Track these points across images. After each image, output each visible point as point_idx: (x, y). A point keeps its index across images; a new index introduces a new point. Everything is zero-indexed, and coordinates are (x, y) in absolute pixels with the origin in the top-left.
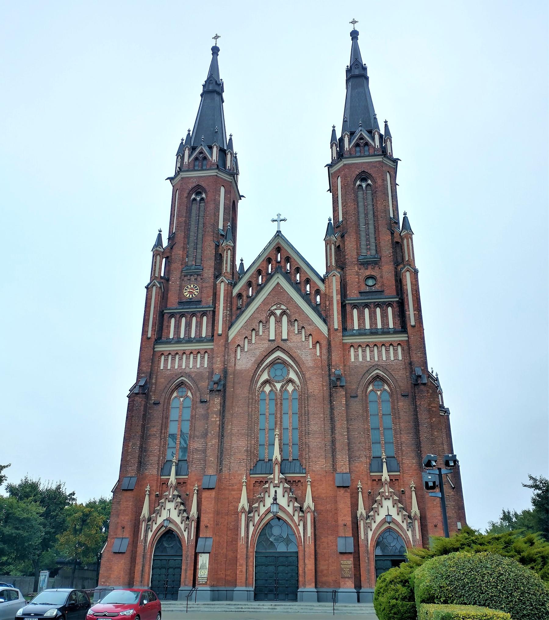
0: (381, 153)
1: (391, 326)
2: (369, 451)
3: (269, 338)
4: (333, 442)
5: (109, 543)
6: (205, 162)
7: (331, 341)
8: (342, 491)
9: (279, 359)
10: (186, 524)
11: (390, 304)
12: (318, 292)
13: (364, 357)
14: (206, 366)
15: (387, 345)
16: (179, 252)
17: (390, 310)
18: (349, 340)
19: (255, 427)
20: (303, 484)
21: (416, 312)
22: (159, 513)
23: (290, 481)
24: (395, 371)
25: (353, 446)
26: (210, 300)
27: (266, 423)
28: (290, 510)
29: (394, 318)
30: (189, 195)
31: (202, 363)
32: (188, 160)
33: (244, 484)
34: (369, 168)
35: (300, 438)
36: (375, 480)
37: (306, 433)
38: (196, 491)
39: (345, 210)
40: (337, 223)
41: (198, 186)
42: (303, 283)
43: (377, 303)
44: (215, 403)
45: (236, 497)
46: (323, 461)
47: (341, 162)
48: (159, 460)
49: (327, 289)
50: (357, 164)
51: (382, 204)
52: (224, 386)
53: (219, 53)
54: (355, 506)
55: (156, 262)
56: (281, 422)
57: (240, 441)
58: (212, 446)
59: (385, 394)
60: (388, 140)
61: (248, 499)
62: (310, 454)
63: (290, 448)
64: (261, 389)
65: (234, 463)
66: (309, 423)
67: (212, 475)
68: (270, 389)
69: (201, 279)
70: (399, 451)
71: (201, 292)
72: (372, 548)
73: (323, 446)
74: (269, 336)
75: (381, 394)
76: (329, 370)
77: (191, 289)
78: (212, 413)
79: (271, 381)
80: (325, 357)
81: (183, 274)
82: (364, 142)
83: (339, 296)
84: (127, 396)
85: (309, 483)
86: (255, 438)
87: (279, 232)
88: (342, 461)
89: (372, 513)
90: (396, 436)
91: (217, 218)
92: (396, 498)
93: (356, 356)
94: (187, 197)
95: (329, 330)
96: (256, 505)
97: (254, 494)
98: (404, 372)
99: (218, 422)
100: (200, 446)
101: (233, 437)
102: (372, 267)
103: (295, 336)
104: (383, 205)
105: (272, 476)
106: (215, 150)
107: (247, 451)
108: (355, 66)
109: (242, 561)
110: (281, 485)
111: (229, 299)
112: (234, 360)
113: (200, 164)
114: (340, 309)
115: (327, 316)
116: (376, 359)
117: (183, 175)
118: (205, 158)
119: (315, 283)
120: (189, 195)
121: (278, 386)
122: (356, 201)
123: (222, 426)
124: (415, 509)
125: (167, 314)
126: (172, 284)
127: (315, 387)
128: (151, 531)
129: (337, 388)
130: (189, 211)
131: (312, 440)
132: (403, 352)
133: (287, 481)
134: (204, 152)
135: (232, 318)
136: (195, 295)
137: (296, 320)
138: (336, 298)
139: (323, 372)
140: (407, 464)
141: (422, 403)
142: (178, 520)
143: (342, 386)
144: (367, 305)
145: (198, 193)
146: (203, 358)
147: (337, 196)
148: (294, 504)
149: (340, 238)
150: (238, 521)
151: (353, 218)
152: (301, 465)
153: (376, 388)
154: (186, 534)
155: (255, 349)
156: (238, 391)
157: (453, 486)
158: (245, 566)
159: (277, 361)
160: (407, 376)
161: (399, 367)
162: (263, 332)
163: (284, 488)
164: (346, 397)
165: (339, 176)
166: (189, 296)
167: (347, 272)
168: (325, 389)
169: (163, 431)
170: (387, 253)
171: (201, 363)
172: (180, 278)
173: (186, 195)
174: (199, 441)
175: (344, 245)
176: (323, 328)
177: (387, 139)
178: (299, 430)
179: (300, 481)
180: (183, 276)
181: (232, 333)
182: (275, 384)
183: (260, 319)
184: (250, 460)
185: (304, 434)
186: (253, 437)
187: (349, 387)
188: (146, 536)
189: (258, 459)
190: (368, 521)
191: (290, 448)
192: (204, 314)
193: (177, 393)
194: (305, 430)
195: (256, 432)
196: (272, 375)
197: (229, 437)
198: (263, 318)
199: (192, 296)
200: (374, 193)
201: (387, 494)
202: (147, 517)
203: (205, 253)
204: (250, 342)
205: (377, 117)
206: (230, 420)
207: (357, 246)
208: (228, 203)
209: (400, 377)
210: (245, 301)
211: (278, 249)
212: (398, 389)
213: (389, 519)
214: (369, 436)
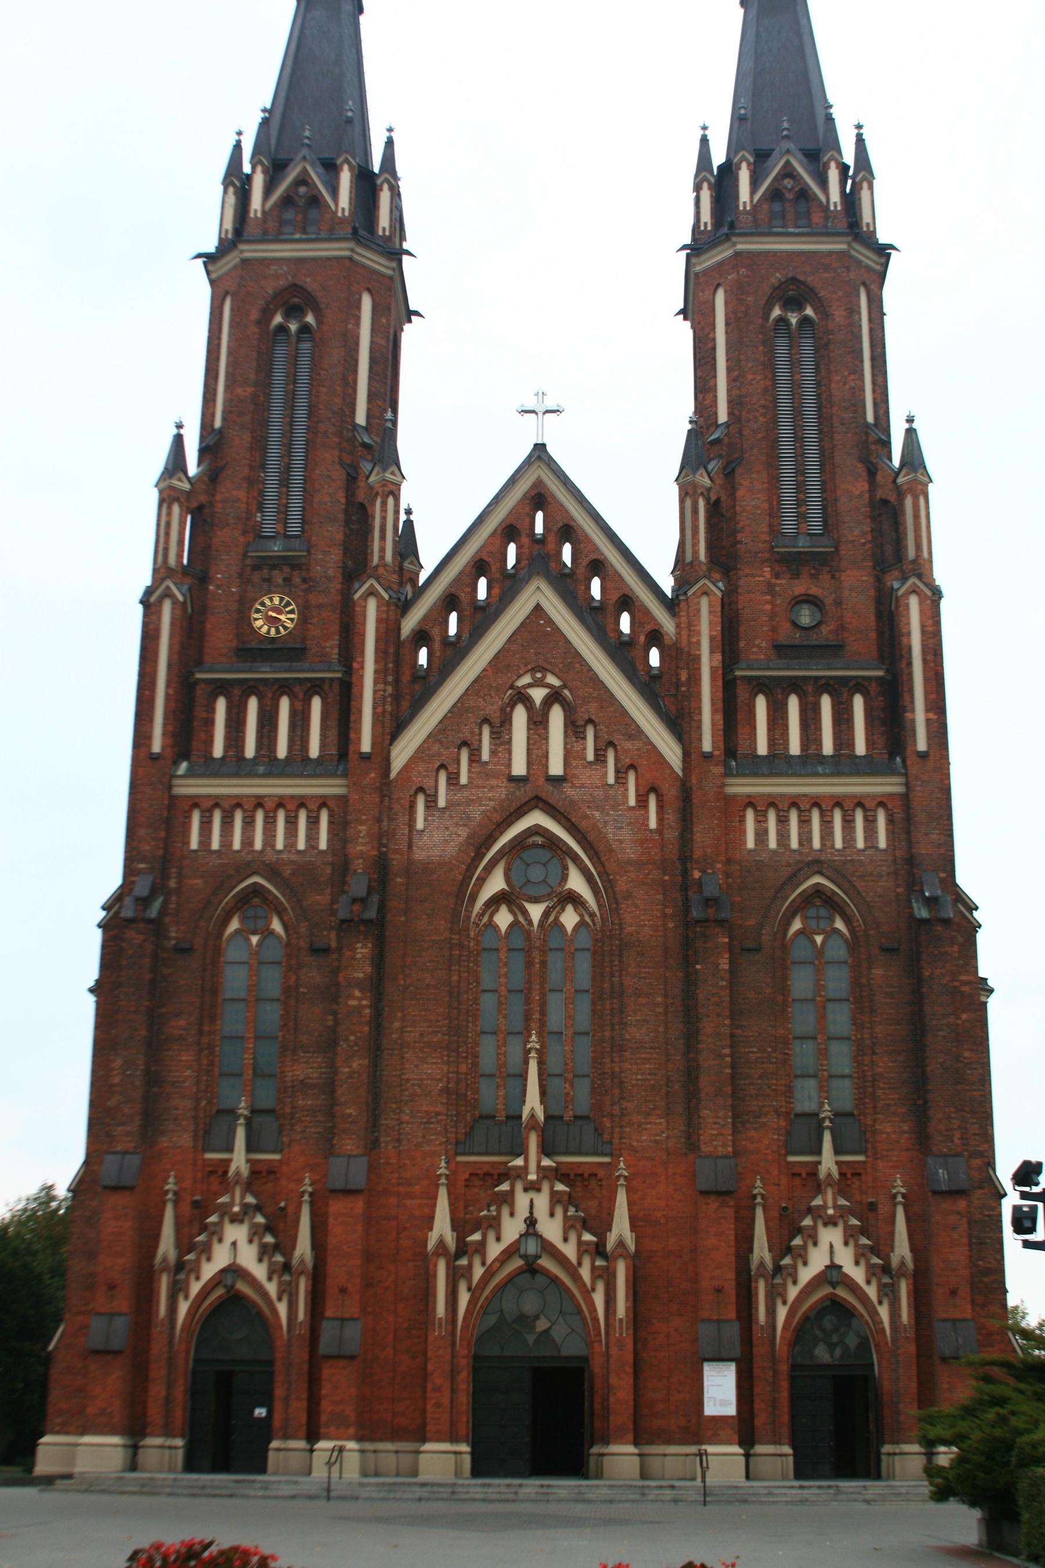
1: (860, 748)
2: (786, 1097)
3: (510, 772)
4: (691, 1073)
6: (313, 213)
7: (691, 788)
8: (713, 1204)
9: (537, 833)
10: (280, 1284)
11: (859, 686)
12: (655, 637)
14: (323, 845)
15: (848, 805)
16: (235, 493)
17: (316, 703)
18: (741, 787)
19: (467, 1027)
20: (603, 1183)
21: (931, 716)
22: (206, 1251)
23: (568, 1175)
24: (866, 878)
25: (745, 1084)
26: (332, 647)
27: (500, 1016)
30: (267, 314)
32: (263, 205)
33: (443, 1180)
35: (594, 1060)
36: (800, 1175)
38: (306, 1197)
41: (295, 288)
42: (551, 538)
43: (823, 681)
44: (359, 956)
46: (661, 1123)
47: (726, 245)
48: (196, 1108)
49: (684, 632)
50: (774, 254)
51: (845, 384)
52: (382, 908)
54: (745, 1242)
55: (168, 524)
56: (543, 1013)
57: (427, 1063)
58: (351, 1077)
59: (836, 943)
60: (865, 185)
61: (453, 1220)
62: (625, 1104)
63: (567, 1085)
64: (485, 919)
65: (412, 1123)
66: (625, 1020)
67: (354, 1156)
69: (304, 580)
70: (867, 1100)
71: (304, 620)
72: (785, 1348)
73: (662, 1082)
74: (509, 765)
76: (685, 873)
77: (275, 609)
79: (514, 898)
80: (672, 835)
81: (248, 562)
82: (797, 189)
83: (718, 657)
85: (622, 1181)
86: (470, 1057)
87: (540, 449)
88: (715, 1126)
89: (787, 1261)
90: (860, 1058)
91: (350, 391)
92: (854, 1222)
93: (761, 835)
94: (258, 322)
95: (686, 755)
96: (476, 1237)
97: (466, 1207)
100: (312, 1073)
101: (407, 1053)
102: (813, 571)
103: (587, 767)
104: (847, 387)
105: (519, 1162)
106: (345, 178)
107: (446, 1091)
109: (438, 1379)
110: (546, 1187)
111: (391, 650)
112: (406, 832)
113: (300, 217)
116: (816, 844)
117: (250, 251)
118: (315, 200)
119: (647, 612)
120: (267, 314)
121: (535, 912)
122: (769, 366)
123: (377, 1022)
124: (902, 1249)
125: (203, 685)
127: (643, 920)
129: (707, 924)
130: (266, 366)
131: (629, 1067)
132: (890, 827)
133: (559, 1174)
134: (310, 181)
135: (398, 704)
136: (285, 628)
137: (590, 721)
139: (667, 878)
140: (888, 1133)
141: (938, 972)
143: (720, 922)
144: (795, 686)
147: (710, 345)
148: (579, 1237)
149: (721, 476)
150: (429, 1279)
151: (762, 419)
152: (598, 1132)
154: (282, 1308)
155: (469, 802)
158: (447, 1393)
159: (531, 840)
160: (898, 895)
162: (493, 753)
163: (553, 1194)
164: (731, 952)
165: (719, 285)
166: (268, 632)
167: (741, 583)
168: (671, 925)
169: (206, 1028)
170: (856, 532)
172: (241, 575)
173: (255, 314)
174: (311, 1060)
175: (734, 499)
176: (671, 751)
177: (861, 182)
178: (593, 1036)
179: (596, 1175)
181: (402, 753)
184: (456, 1115)
185: (608, 1050)
186: (464, 1055)
187: (739, 922)
188: (173, 1309)
189: (477, 1113)
190: (778, 1280)
191: (567, 1085)
192: (315, 687)
193: (241, 922)
195: (470, 1040)
196: (518, 880)
197: (395, 1052)
198: (492, 710)
199: (278, 631)
200: (821, 349)
201: (830, 1212)
203: (316, 500)
204: (453, 779)
205: (835, 112)
206: (399, 1004)
207: (771, 504)
208: (383, 342)
209: (880, 896)
210: (438, 654)
211: (538, 499)
212: (872, 932)
214: (786, 1057)
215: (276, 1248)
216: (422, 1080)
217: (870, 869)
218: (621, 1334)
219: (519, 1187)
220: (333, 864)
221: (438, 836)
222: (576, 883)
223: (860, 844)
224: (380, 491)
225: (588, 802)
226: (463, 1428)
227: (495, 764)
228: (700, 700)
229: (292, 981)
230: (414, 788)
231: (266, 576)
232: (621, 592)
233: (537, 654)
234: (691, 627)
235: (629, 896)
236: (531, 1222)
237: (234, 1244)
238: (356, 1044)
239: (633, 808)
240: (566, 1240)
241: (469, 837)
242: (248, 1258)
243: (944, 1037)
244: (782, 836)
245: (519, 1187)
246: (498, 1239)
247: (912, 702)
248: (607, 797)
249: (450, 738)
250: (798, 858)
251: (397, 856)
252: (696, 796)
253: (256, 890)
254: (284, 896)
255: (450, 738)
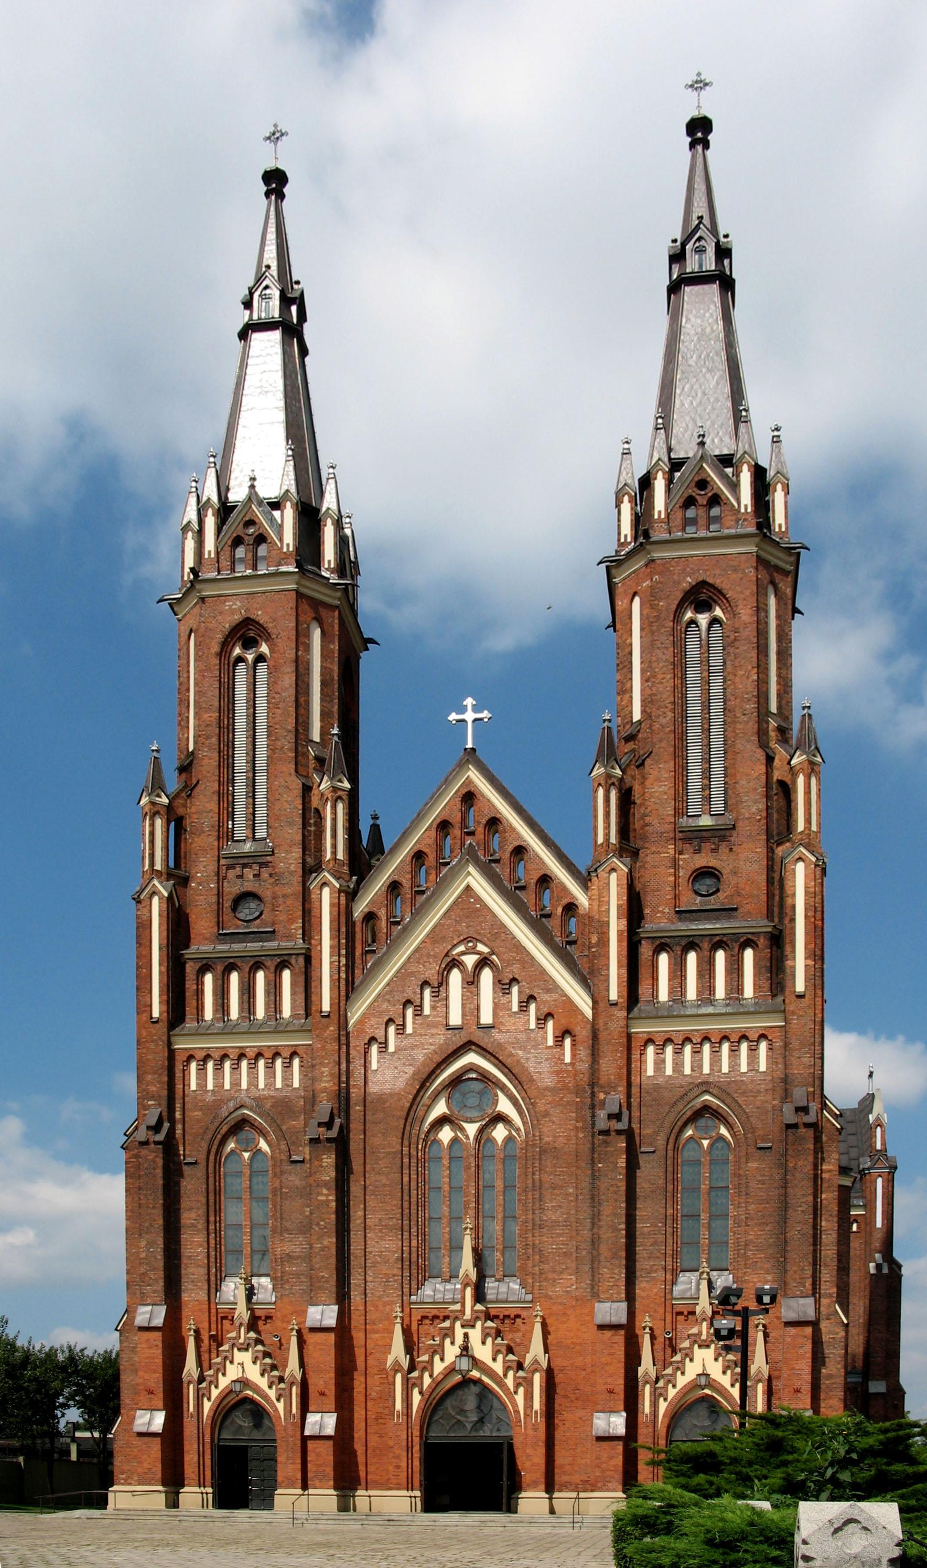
0: (752, 529)
4: (595, 1242)
5: (125, 1417)
13: (678, 1065)
14: (296, 1084)
16: (208, 805)
17: (749, 954)
28: (498, 1367)
29: (757, 975)
31: (287, 1078)
34: (718, 572)
37: (534, 1225)
39: (649, 692)
40: (628, 727)
43: (718, 938)
45: (379, 1343)
53: (285, 190)
58: (323, 1251)
68: (452, 1134)
69: (271, 875)
75: (711, 1146)
76: (593, 1094)
78: (318, 1185)
80: (584, 1066)
83: (624, 922)
84: (122, 1147)
93: (660, 1064)
95: (595, 1003)
98: (769, 1097)
99: (334, 1204)
105: (457, 1307)
108: (697, 244)
110: (479, 1324)
112: (363, 1072)
114: (625, 953)
115: (592, 972)
121: (472, 1129)
126: (199, 890)
128: (209, 1399)
134: (257, 521)
138: (615, 926)
140: (754, 1282)
141: (800, 1163)
142: (263, 1383)
145: (249, 644)
146: (288, 1066)
147: (627, 650)
153: (698, 1134)
154: (280, 1406)
155: (413, 1047)
156: (375, 1140)
157: (846, 1322)
160: (774, 1106)
161: (757, 1087)
162: (433, 1008)
165: (635, 594)
168: (581, 1135)
170: (754, 810)
171: (284, 1079)
173: (216, 648)
176: (583, 1002)
180: (224, 868)
182: (465, 1125)
183: (422, 978)
194: (533, 1220)
198: (431, 975)
202: (196, 1376)
203: (277, 808)
213: (703, 1381)
215: (274, 1367)
216: (382, 1252)
217: (750, 1087)
218: (536, 1420)
219: (458, 1324)
220: (304, 1097)
221: (389, 1075)
222: (504, 1106)
223: (744, 1068)
224: (329, 796)
225: (513, 1043)
226: (417, 1483)
227: (435, 1016)
228: (608, 958)
229: (277, 1184)
230: (368, 1038)
231: (240, 873)
232: (542, 873)
233: (467, 927)
234: (602, 900)
235: (546, 1114)
236: (465, 1349)
237: (242, 1364)
238: (325, 1227)
239: (550, 1047)
240: (494, 1359)
241: (414, 1074)
242: (253, 1373)
243: (803, 1211)
244: (677, 1064)
245: (458, 1324)
246: (442, 1359)
247: (794, 951)
248: (529, 1039)
249: (396, 998)
250: (690, 1080)
251: (356, 1090)
252: (603, 1035)
253: (706, 1108)
254: (266, 1122)
255: (396, 998)
